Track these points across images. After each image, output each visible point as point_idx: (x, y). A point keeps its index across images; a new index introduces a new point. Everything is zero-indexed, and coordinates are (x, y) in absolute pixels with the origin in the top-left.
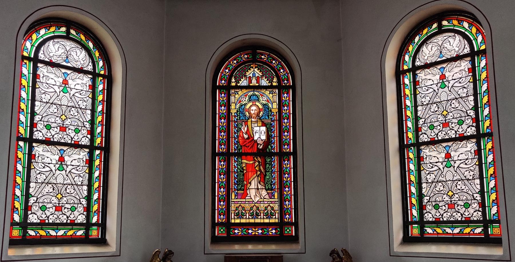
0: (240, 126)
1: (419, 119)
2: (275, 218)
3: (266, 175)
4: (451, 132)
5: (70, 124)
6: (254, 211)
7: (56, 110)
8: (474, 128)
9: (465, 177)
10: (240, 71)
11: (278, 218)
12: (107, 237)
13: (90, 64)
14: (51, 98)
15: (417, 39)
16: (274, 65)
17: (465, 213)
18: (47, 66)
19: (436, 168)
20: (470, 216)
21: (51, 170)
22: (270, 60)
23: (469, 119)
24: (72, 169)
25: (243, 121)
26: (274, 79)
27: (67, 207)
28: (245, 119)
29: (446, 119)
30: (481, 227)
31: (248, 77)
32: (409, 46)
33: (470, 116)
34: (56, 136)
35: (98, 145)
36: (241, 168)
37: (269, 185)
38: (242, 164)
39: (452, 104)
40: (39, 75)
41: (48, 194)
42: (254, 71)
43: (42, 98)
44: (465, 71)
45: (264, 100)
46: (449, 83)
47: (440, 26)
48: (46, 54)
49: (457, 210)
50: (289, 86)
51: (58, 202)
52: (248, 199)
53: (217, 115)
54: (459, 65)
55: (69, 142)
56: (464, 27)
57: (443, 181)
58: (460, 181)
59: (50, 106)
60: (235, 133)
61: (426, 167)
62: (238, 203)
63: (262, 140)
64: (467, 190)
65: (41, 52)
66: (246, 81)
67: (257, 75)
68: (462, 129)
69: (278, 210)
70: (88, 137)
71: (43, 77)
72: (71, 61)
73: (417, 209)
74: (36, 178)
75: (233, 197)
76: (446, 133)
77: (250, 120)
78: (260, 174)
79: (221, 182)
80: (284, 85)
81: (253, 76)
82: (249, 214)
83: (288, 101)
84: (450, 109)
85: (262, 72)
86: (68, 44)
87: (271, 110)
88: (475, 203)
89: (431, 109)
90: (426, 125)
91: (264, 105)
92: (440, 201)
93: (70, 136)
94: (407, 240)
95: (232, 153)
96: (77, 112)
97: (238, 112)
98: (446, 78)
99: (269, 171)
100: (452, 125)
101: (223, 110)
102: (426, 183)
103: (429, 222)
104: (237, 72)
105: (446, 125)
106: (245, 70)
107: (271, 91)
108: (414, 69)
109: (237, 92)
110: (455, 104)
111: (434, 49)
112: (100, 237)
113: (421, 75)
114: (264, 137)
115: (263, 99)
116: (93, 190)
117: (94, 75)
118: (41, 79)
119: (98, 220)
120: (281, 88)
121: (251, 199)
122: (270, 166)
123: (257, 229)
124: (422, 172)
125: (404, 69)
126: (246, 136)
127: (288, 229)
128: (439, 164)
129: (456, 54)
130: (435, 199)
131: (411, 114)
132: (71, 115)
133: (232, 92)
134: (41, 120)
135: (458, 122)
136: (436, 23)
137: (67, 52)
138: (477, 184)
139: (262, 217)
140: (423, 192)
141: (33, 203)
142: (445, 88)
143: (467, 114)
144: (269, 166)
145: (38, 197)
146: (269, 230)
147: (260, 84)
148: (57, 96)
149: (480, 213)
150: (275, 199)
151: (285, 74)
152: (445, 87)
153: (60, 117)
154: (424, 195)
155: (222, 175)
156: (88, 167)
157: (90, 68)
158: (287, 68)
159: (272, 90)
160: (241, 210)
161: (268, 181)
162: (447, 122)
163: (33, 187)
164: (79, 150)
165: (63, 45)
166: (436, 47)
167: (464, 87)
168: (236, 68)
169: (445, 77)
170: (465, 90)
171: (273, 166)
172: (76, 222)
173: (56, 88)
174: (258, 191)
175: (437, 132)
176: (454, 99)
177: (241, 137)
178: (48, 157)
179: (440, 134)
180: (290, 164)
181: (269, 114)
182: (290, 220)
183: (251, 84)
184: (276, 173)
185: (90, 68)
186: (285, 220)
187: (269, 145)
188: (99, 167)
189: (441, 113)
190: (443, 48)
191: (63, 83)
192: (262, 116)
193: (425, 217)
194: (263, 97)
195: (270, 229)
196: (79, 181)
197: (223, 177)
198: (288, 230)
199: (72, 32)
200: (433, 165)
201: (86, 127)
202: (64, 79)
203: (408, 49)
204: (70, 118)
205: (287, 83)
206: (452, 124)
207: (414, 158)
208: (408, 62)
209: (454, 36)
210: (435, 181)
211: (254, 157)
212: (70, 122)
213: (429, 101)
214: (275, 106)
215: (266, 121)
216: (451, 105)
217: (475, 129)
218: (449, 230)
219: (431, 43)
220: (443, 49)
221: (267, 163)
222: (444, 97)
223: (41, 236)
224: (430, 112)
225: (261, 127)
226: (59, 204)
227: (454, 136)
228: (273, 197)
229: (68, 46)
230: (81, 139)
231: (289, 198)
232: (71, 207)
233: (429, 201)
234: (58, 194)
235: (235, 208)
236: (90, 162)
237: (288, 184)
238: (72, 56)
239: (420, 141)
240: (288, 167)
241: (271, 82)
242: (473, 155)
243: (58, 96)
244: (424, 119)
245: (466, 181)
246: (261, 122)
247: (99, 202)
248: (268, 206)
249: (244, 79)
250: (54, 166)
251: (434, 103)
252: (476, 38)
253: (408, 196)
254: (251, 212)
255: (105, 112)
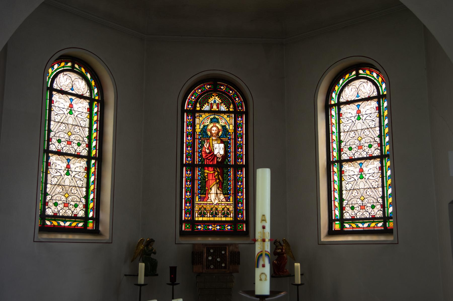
0: (203, 143)
1: (341, 142)
2: (231, 217)
3: (223, 183)
4: (364, 153)
5: (74, 139)
6: (213, 211)
7: (64, 128)
8: (379, 151)
9: (372, 186)
10: (204, 99)
11: (233, 217)
12: (100, 228)
13: (88, 91)
14: (61, 118)
15: (341, 81)
16: (231, 94)
17: (371, 212)
18: (59, 93)
19: (352, 179)
20: (375, 214)
21: (61, 175)
22: (228, 90)
23: (376, 144)
24: (76, 174)
25: (206, 139)
26: (231, 106)
27: (72, 204)
28: (208, 138)
29: (361, 143)
30: (382, 222)
31: (210, 103)
32: (336, 86)
33: (377, 141)
34: (64, 148)
35: (94, 156)
36: (203, 176)
37: (226, 191)
38: (205, 173)
39: (365, 133)
40: (53, 101)
41: (59, 193)
42: (215, 98)
43: (55, 119)
44: (374, 109)
45: (223, 122)
46: (363, 116)
47: (358, 74)
48: (58, 84)
49: (366, 210)
50: (243, 111)
51: (66, 200)
52: (209, 201)
53: (185, 133)
54: (370, 104)
55: (74, 153)
56: (373, 76)
57: (358, 189)
58: (369, 189)
59: (60, 125)
60: (199, 148)
61: (345, 178)
62: (201, 205)
63: (221, 155)
64: (374, 196)
65: (55, 82)
66: (208, 107)
67: (217, 102)
68: (371, 151)
69: (233, 211)
70: (86, 150)
71: (56, 102)
72: (75, 89)
73: (339, 210)
74: (51, 180)
75: (197, 200)
76: (360, 154)
77: (211, 138)
78: (218, 181)
79: (188, 188)
80: (238, 110)
81: (214, 103)
82: (209, 213)
83: (242, 124)
84: (363, 136)
85: (221, 99)
86: (73, 75)
87: (228, 131)
88: (378, 205)
89: (350, 135)
90: (346, 147)
91: (224, 127)
92: (355, 204)
93: (74, 148)
94: (331, 232)
95: (196, 164)
96: (79, 130)
97: (202, 132)
98: (361, 113)
99: (226, 180)
100: (365, 148)
101: (189, 129)
102: (346, 190)
103: (347, 220)
104: (201, 99)
105: (360, 147)
106: (208, 98)
107: (228, 115)
108: (339, 104)
109: (201, 115)
110: (367, 132)
111: (353, 90)
112: (94, 229)
113: (344, 109)
114: (222, 152)
115: (222, 122)
116: (90, 192)
117: (91, 100)
118: (55, 103)
119: (93, 215)
120: (237, 114)
121: (211, 201)
122: (227, 176)
123: (215, 226)
124: (343, 182)
125: (332, 104)
126: (208, 151)
127: (240, 226)
128: (355, 176)
129: (368, 95)
130: (352, 202)
131: (336, 138)
132: (75, 132)
133: (197, 115)
134: (54, 136)
135: (368, 146)
136: (355, 71)
137: (73, 82)
138: (380, 191)
139: (220, 216)
140: (343, 197)
141: (49, 200)
142: (360, 120)
143: (375, 140)
144: (226, 175)
145: (53, 195)
146: (226, 226)
147: (220, 109)
148: (65, 117)
149: (381, 212)
150: (230, 202)
151: (240, 102)
152: (360, 120)
153: (67, 133)
154: (344, 199)
155: (188, 182)
156: (86, 173)
157: (88, 95)
158: (241, 96)
159: (229, 114)
160: (204, 211)
161: (225, 188)
162: (361, 145)
163: (49, 188)
164: (80, 160)
165: (69, 76)
166: (355, 89)
167: (373, 121)
168: (200, 96)
169: (360, 112)
170: (374, 123)
171: (230, 176)
172: (78, 216)
173: (64, 110)
174: (217, 195)
175: (354, 152)
176: (366, 129)
177: (204, 152)
178: (59, 165)
179: (356, 154)
180: (243, 174)
181: (226, 133)
182: (242, 219)
183: (212, 109)
184: (231, 181)
185: (88, 95)
186: (238, 219)
187: (226, 158)
188: (94, 173)
189: (357, 138)
190: (360, 90)
191: (69, 107)
192: (221, 135)
193: (345, 216)
194: (222, 120)
195: (227, 226)
196: (80, 184)
197: (189, 183)
198: (240, 227)
199: (76, 66)
200: (351, 177)
201: (85, 142)
202: (71, 103)
203: (335, 89)
204: (74, 134)
205: (241, 109)
206: (364, 147)
207: (338, 171)
208: (334, 98)
209: (367, 82)
210: (352, 189)
211: (214, 168)
212: (74, 137)
213: (349, 129)
214: (231, 127)
215: (224, 139)
216: (364, 133)
217: (379, 151)
218: (360, 225)
219: (351, 86)
220: (359, 91)
221: (225, 173)
222: (359, 127)
223: (54, 225)
224: (349, 137)
225: (220, 144)
226: (66, 201)
227: (365, 156)
228: (229, 200)
229: (73, 78)
230: (82, 151)
231: (241, 201)
232: (75, 204)
233: (347, 204)
234: (66, 193)
235: (199, 208)
236: (88, 169)
237: (241, 190)
238: (76, 86)
239: (342, 159)
240: (241, 176)
241: (228, 108)
242: (378, 170)
243: (66, 117)
244: (345, 142)
245: (373, 189)
246: (220, 140)
247: (94, 201)
248: (225, 207)
249: (207, 105)
250: (63, 172)
251: (353, 131)
252: (381, 85)
253: (333, 200)
254: (212, 212)
255: (98, 130)
